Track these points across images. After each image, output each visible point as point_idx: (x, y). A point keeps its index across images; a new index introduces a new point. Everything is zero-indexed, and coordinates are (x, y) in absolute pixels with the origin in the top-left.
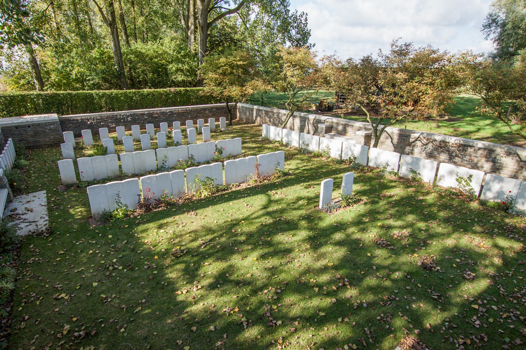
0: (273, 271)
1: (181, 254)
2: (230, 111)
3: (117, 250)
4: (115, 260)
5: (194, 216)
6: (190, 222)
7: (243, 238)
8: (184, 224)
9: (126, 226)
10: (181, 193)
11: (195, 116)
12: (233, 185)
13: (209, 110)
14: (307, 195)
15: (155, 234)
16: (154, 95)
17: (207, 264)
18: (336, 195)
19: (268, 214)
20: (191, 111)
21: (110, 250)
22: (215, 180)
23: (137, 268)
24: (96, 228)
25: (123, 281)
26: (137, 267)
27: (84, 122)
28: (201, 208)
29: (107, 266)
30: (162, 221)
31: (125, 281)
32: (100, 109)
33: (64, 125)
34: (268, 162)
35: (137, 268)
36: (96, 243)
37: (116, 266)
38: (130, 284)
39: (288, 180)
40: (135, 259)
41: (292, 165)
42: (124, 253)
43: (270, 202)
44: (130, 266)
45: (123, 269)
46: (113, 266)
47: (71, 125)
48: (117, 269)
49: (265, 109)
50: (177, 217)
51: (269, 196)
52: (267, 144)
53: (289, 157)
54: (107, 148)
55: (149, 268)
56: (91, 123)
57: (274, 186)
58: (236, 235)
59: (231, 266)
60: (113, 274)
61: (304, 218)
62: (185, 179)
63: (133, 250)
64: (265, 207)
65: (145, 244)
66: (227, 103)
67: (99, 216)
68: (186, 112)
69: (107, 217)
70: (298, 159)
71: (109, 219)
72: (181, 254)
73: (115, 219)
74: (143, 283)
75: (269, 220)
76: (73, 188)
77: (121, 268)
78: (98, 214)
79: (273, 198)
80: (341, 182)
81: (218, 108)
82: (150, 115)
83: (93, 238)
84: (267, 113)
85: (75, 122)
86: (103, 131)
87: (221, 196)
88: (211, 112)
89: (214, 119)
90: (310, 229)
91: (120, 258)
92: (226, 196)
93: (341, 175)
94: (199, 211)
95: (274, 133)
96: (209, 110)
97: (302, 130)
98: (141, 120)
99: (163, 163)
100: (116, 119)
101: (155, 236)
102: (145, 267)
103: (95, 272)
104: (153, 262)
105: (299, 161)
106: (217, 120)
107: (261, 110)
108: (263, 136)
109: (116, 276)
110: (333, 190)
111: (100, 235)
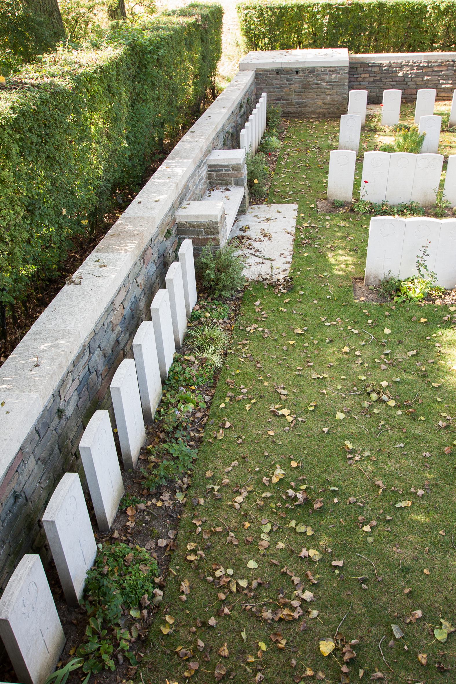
3: (394, 365)
9: (423, 320)
23: (423, 418)
26: (424, 415)
29: (369, 389)
33: (355, 74)
35: (423, 418)
36: (359, 335)
37: (385, 397)
38: (402, 445)
42: (406, 376)
45: (397, 407)
47: (367, 75)
48: (384, 402)
67: (377, 282)
69: (390, 289)
71: (393, 293)
73: (403, 298)
76: (342, 210)
77: (392, 403)
85: (376, 69)
91: (396, 382)
102: (441, 423)
111: (370, 321)
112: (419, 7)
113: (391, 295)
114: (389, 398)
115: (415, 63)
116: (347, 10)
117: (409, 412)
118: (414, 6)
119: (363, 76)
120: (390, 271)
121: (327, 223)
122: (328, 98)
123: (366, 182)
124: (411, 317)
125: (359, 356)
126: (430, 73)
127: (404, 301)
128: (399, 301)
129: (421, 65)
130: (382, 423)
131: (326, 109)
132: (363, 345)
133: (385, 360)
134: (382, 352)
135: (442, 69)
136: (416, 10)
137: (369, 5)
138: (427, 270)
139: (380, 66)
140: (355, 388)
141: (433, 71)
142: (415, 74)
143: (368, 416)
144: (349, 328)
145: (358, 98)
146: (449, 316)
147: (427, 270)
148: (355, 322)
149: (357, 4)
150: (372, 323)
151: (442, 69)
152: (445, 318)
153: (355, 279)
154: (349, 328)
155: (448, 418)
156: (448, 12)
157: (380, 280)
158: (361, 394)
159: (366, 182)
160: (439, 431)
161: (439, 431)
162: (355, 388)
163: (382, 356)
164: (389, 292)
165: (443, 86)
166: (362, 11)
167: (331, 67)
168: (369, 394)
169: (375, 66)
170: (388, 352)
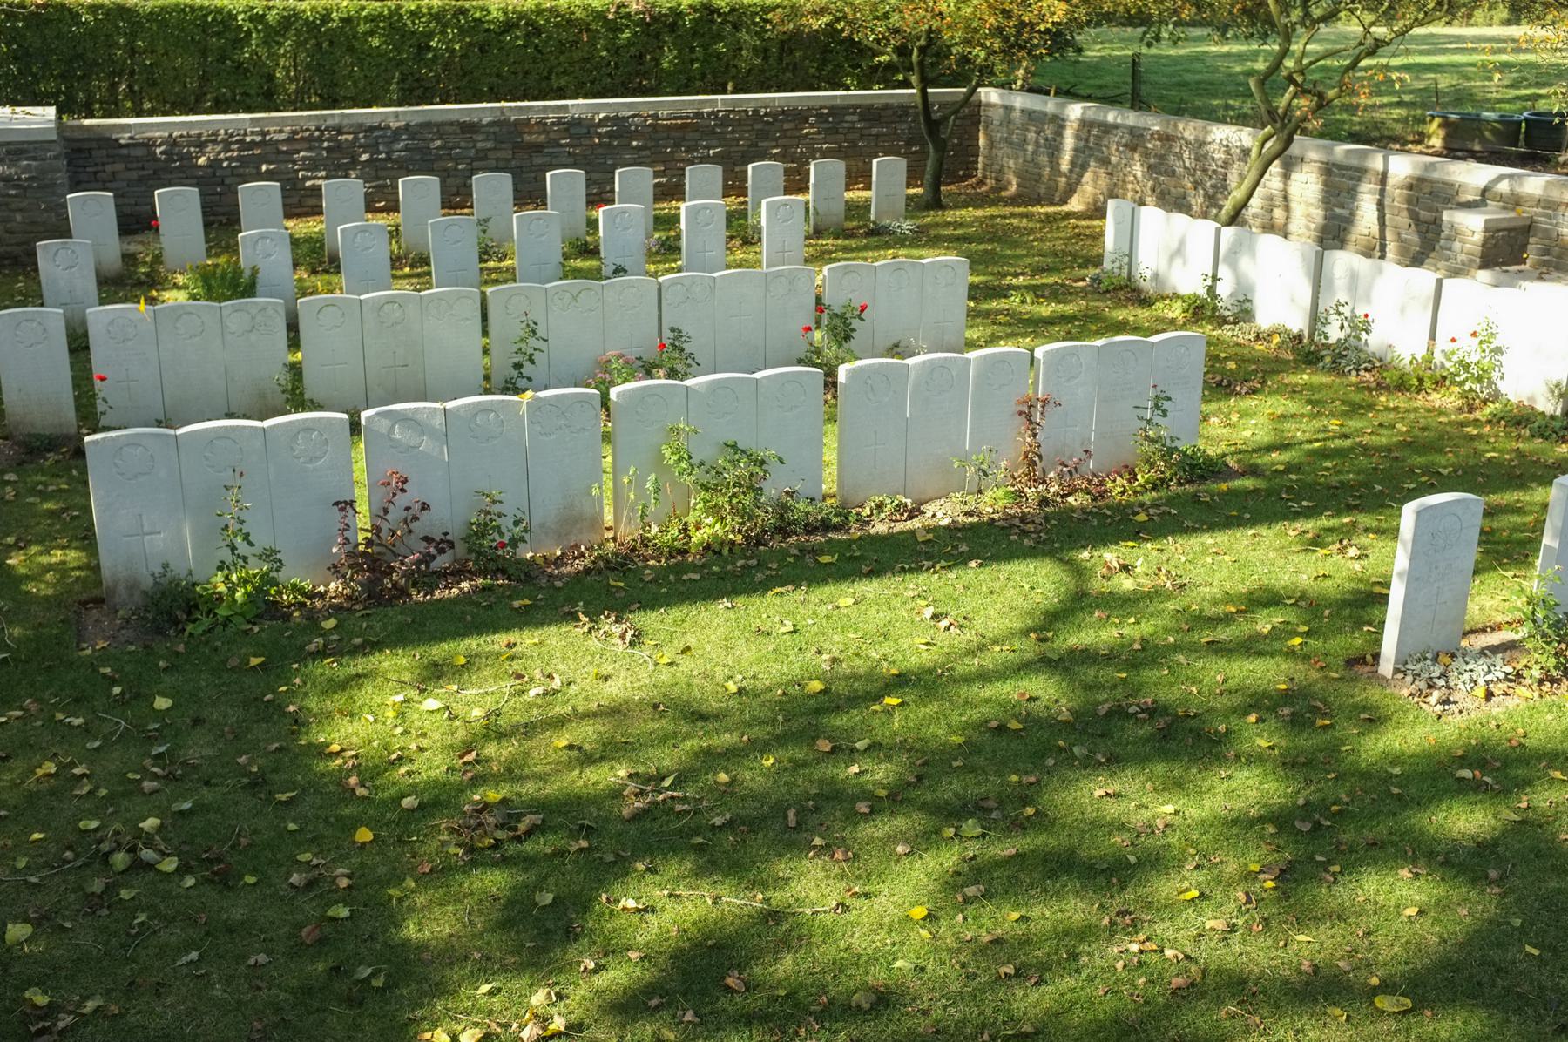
0: (1023, 961)
1: (500, 834)
2: (933, 126)
3: (177, 775)
4: (150, 823)
5: (620, 647)
6: (586, 666)
7: (881, 773)
8: (556, 683)
9: (255, 661)
10: (580, 519)
11: (735, 147)
12: (880, 506)
13: (819, 116)
14: (1304, 580)
15: (390, 714)
16: (538, 31)
17: (631, 904)
18: (1498, 600)
19: (1047, 664)
20: (725, 122)
21: (144, 771)
22: (773, 465)
23: (251, 880)
24: (105, 657)
25: (164, 936)
26: (254, 872)
27: (182, 157)
28: (667, 601)
29: (105, 847)
30: (439, 651)
31: (174, 935)
32: (268, 99)
33: (84, 160)
34: (1096, 400)
35: (251, 880)
36: (86, 730)
37: (147, 854)
38: (194, 955)
39: (1204, 495)
40: (255, 832)
41: (1241, 427)
42: (207, 795)
43: (1078, 604)
44: (219, 860)
45: (183, 870)
46: (132, 850)
47: (119, 167)
48: (150, 866)
49: (1132, 118)
50: (526, 639)
51: (1078, 571)
52: (1321, 387)
53: (1229, 378)
54: (255, 272)
55: (311, 884)
56: (214, 164)
57: (1116, 524)
58: (842, 751)
59: (772, 916)
60: (125, 894)
61: (1261, 703)
62: (607, 450)
63: (256, 784)
64: (1054, 618)
65: (322, 752)
66: (926, 82)
67: (138, 598)
68: (696, 128)
69: (174, 607)
70: (1293, 392)
71: (181, 616)
72: (500, 834)
73: (206, 622)
74: (262, 958)
75: (1044, 690)
76: (52, 457)
77: (170, 865)
78: (132, 586)
79: (1097, 585)
80: (1539, 527)
81: (871, 114)
82: (508, 131)
83: (79, 702)
84: (1135, 140)
85: (140, 152)
86: (258, 197)
87: (789, 547)
88: (833, 131)
89: (838, 167)
90: (1292, 764)
91: (181, 813)
92: (825, 559)
93: (1538, 495)
94: (652, 620)
95: (1169, 248)
96: (819, 116)
97: (1334, 233)
98: (457, 160)
99: (518, 366)
100: (336, 148)
101: (396, 718)
102: (295, 878)
103: (39, 868)
104: (341, 859)
105: (1291, 406)
106: (858, 176)
107: (1108, 129)
108: (1107, 265)
109: (132, 907)
110: (1476, 572)
111: (117, 690)
112: (219, 18)
113: (176, 622)
114: (163, 854)
115: (232, 136)
116: (37, 19)
117: (216, 873)
118: (206, 16)
119: (109, 168)
120: (165, 566)
121: (8, 489)
122: (19, 217)
123: (103, 379)
124: (224, 662)
125: (84, 775)
126: (274, 157)
127: (210, 630)
128: (200, 630)
129: (248, 139)
130: (142, 917)
131: (18, 244)
132: (97, 749)
133: (155, 769)
134: (147, 754)
135: (297, 147)
136: (210, 25)
137: (93, 9)
138: (251, 544)
139: (149, 144)
140: (69, 854)
141: (279, 152)
142: (237, 159)
143: (105, 912)
144: (60, 716)
145: (92, 210)
146: (320, 640)
147: (251, 544)
148: (77, 701)
149: (62, 7)
150: (123, 693)
151: (297, 147)
152: (312, 647)
153: (84, 603)
154: (60, 716)
155: (315, 861)
156: (287, 29)
157: (144, 592)
158: (86, 865)
159: (103, 379)
160: (293, 898)
161: (293, 898)
162: (69, 854)
163: (148, 762)
164: (169, 614)
165: (308, 183)
166: (79, 24)
167: (9, 143)
168: (107, 855)
169: (135, 145)
170: (162, 749)
